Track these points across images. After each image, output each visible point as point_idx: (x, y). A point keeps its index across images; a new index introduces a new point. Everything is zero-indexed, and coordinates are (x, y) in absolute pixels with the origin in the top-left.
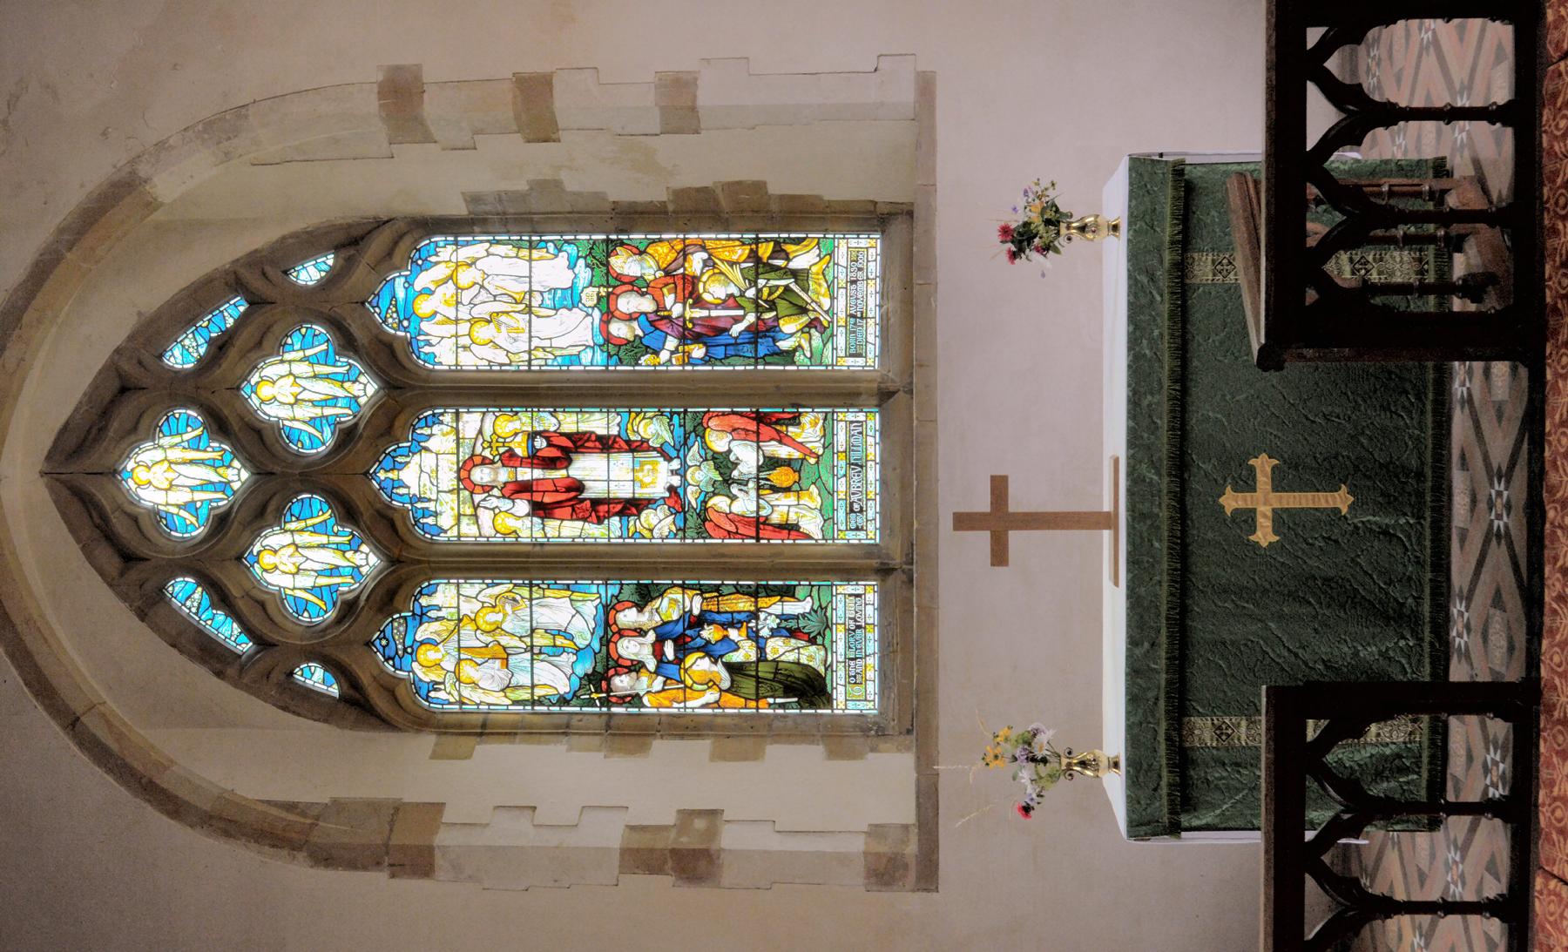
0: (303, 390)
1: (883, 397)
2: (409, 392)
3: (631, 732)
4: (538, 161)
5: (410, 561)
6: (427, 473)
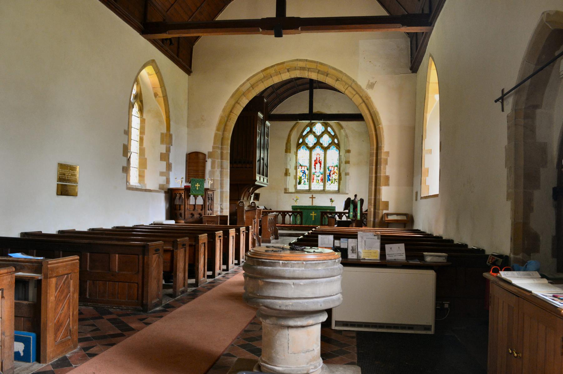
0: (326, 140)
1: (324, 190)
2: (325, 149)
3: (296, 168)
4: (344, 162)
5: (311, 149)
6: (318, 151)
